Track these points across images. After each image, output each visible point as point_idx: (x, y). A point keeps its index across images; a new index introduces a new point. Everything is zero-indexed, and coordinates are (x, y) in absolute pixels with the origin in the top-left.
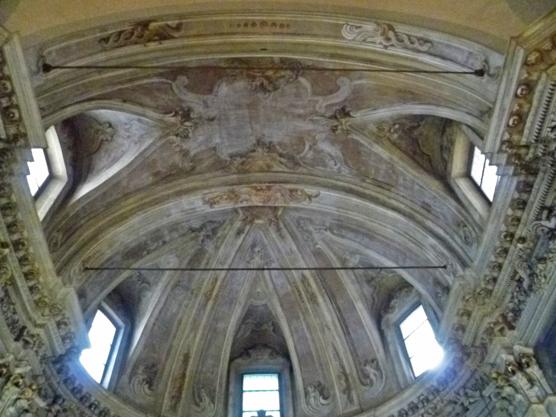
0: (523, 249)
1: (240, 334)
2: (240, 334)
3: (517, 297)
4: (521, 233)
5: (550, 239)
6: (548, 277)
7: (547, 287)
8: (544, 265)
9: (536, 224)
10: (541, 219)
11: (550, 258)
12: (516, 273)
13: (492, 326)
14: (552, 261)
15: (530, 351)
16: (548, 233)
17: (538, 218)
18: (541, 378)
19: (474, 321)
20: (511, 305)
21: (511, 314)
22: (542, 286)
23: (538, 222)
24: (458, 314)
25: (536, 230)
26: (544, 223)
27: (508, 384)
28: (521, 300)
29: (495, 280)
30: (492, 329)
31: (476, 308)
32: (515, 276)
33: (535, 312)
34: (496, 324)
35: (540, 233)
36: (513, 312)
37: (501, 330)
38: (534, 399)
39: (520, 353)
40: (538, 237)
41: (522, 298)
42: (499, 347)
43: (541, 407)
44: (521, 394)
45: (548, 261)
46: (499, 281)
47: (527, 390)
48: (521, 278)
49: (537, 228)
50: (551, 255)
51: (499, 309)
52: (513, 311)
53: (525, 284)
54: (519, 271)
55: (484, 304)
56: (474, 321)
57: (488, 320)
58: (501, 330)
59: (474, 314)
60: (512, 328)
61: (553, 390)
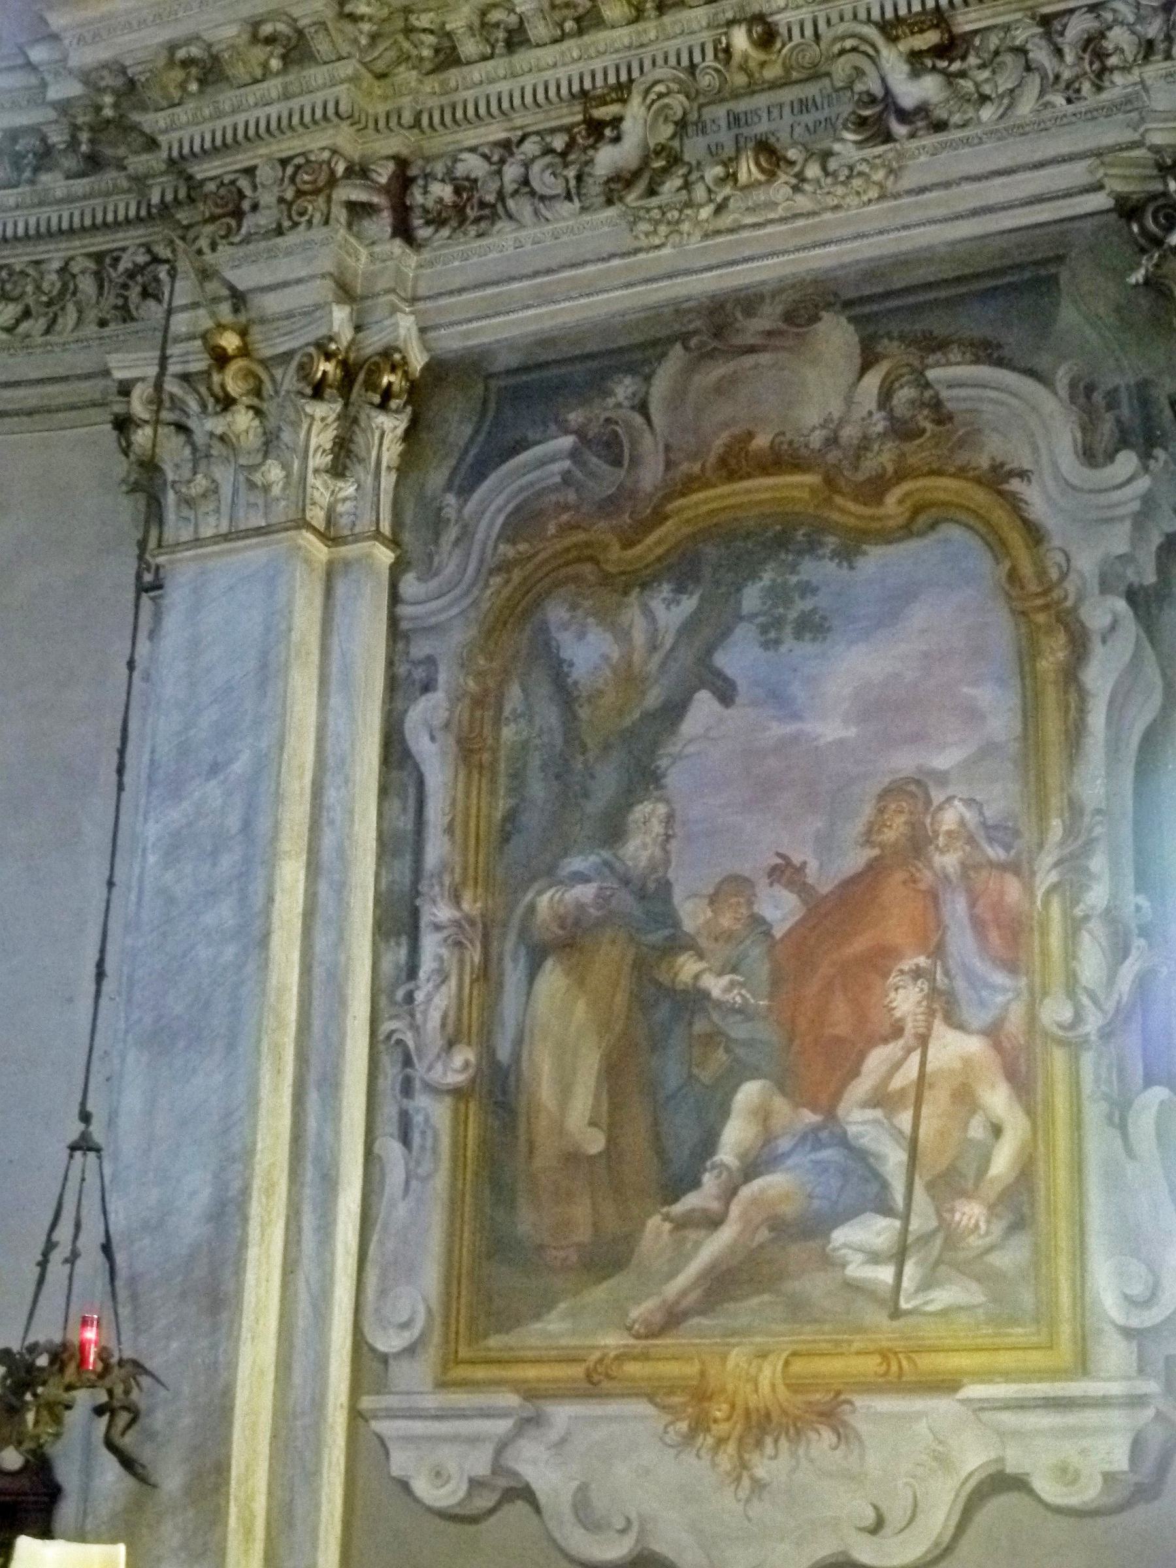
0: (737, 58)
1: (384, 882)
2: (384, 882)
3: (527, 165)
4: (780, 11)
5: (862, 123)
6: (726, 220)
7: (695, 243)
8: (757, 175)
9: (863, 39)
10: (893, 40)
11: (801, 177)
12: (621, 91)
13: (340, 168)
14: (796, 189)
15: (418, 361)
16: (872, 100)
17: (890, 29)
18: (389, 468)
19: (286, 96)
20: (472, 165)
21: (443, 191)
22: (685, 227)
23: (879, 40)
24: (256, 24)
25: (843, 52)
26: (893, 62)
27: (255, 401)
28: (535, 184)
29: (516, 39)
30: (332, 181)
31: (347, 69)
32: (603, 101)
33: (563, 267)
34: (359, 171)
35: (841, 69)
36: (458, 191)
37: (358, 210)
38: (317, 516)
39: (398, 350)
40: (815, 74)
41: (544, 180)
42: (326, 264)
43: (320, 552)
44: (286, 467)
45: (785, 177)
46: (524, 58)
47: (316, 471)
48: (617, 121)
49: (854, 49)
50: (813, 171)
51: (413, 136)
52: (465, 187)
53: (607, 158)
54: (636, 100)
55: (381, 76)
56: (286, 96)
57: (344, 138)
58: (358, 210)
59: (316, 74)
60: (403, 231)
61: (397, 523)
